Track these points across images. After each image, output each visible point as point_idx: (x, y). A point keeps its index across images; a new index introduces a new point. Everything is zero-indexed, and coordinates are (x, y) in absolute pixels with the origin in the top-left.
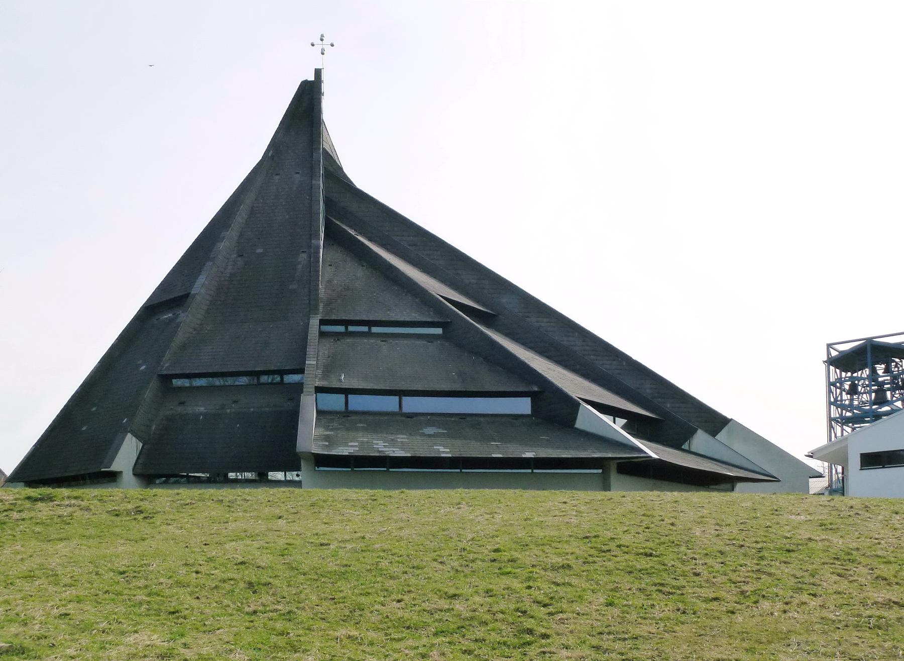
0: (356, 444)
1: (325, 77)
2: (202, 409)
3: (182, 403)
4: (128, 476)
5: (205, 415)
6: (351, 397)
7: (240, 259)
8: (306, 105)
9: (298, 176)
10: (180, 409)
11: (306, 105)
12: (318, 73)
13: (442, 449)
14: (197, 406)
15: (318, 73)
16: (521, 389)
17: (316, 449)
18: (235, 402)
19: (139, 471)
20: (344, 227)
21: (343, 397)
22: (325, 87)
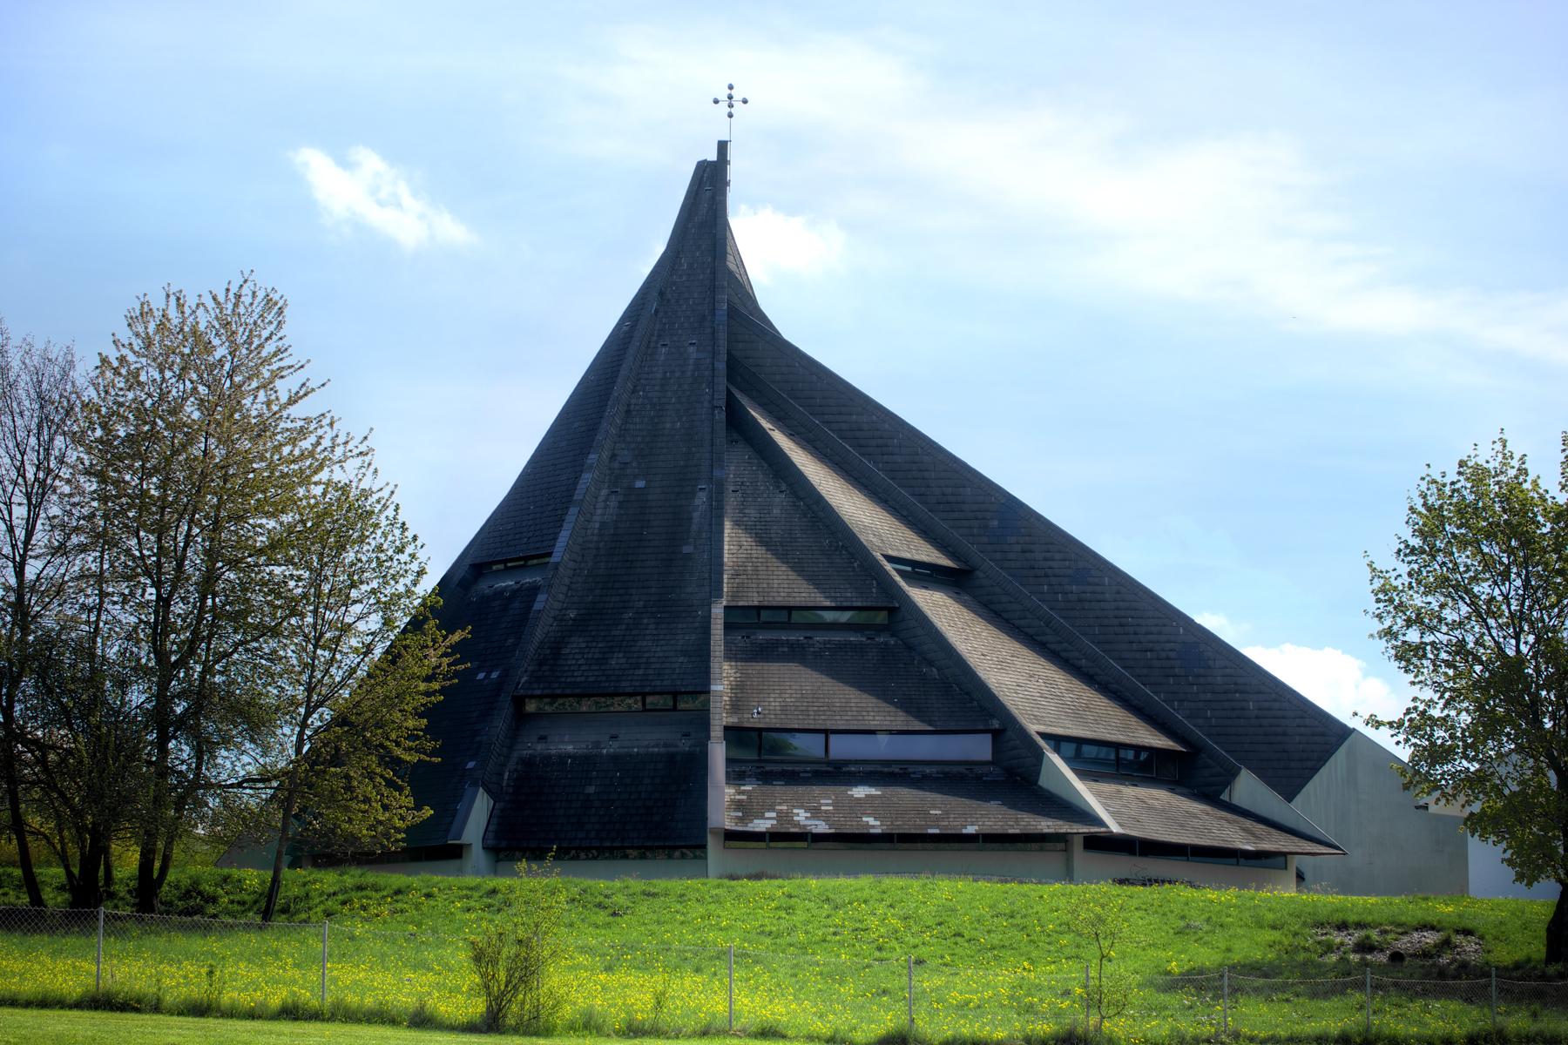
0: (774, 815)
1: (733, 155)
2: (570, 748)
3: (543, 738)
4: (477, 854)
5: (573, 757)
6: (832, 738)
7: (613, 497)
8: (709, 184)
9: (691, 349)
10: (540, 747)
11: (709, 184)
12: (723, 147)
13: (871, 821)
14: (563, 742)
15: (723, 147)
16: (774, 735)
17: (729, 825)
18: (614, 737)
19: (490, 842)
20: (765, 424)
21: (822, 736)
22: (734, 172)
